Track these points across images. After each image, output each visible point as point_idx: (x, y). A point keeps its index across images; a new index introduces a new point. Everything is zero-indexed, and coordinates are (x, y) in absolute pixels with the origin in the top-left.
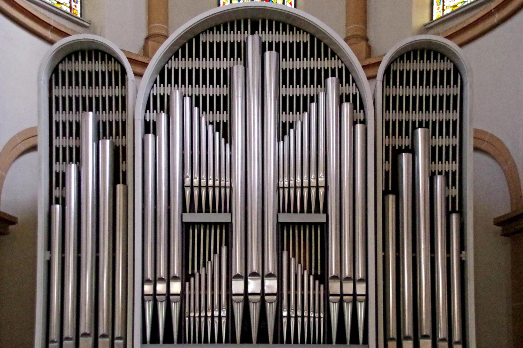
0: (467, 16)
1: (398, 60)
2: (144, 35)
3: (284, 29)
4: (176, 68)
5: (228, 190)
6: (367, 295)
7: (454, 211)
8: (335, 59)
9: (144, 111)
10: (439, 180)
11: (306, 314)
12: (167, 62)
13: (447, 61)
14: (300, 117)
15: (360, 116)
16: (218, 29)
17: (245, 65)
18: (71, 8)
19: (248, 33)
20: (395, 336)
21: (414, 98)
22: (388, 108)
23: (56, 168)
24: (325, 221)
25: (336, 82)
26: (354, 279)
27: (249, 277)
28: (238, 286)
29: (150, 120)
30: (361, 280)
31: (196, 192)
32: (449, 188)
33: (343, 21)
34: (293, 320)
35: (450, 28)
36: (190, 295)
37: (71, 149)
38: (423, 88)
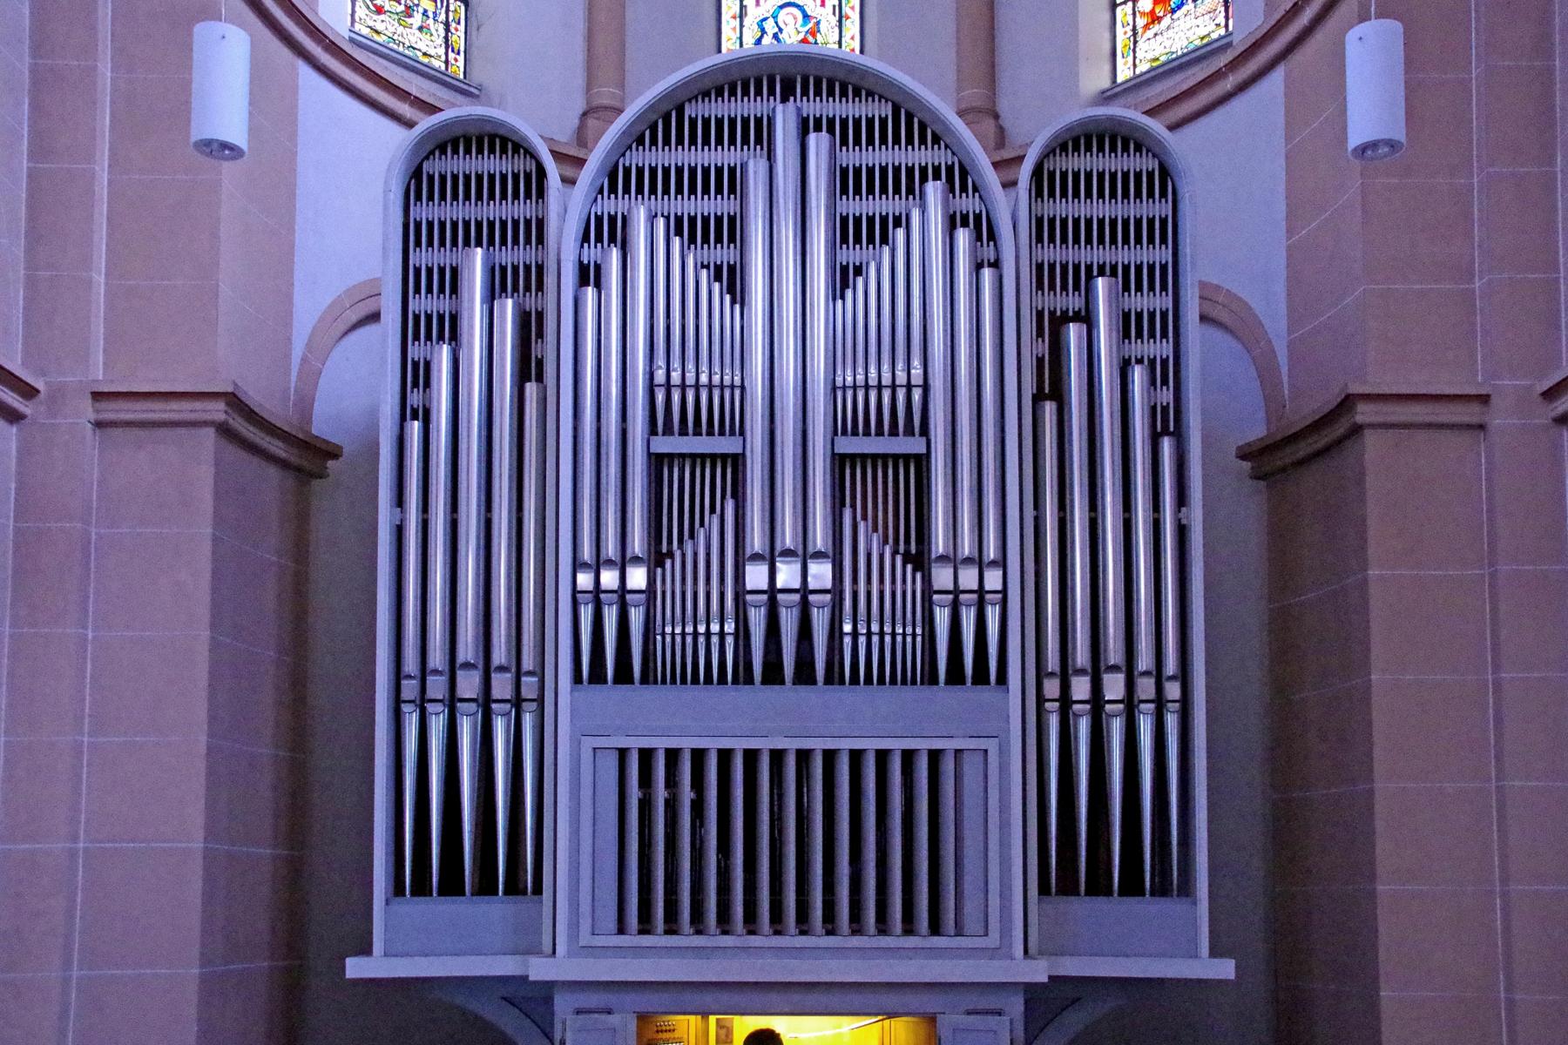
0: (1179, 77)
1: (1058, 151)
2: (580, 106)
3: (844, 94)
4: (640, 165)
5: (737, 393)
6: (1004, 591)
7: (1165, 432)
8: (939, 148)
9: (579, 243)
10: (1138, 375)
11: (888, 629)
12: (623, 155)
13: (1147, 156)
14: (874, 254)
15: (988, 253)
16: (720, 93)
17: (771, 157)
18: (447, 62)
19: (775, 100)
20: (1057, 669)
21: (1089, 222)
22: (1040, 239)
23: (413, 353)
24: (924, 451)
25: (943, 191)
26: (979, 562)
27: (778, 559)
28: (756, 576)
29: (589, 262)
30: (993, 563)
31: (676, 397)
32: (1155, 389)
33: (951, 76)
34: (862, 640)
35: (1147, 98)
36: (664, 593)
37: (441, 317)
38: (1104, 203)
